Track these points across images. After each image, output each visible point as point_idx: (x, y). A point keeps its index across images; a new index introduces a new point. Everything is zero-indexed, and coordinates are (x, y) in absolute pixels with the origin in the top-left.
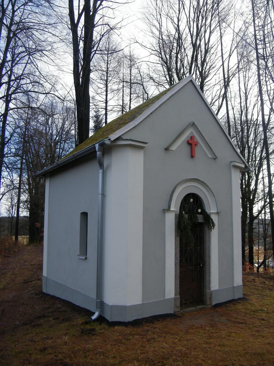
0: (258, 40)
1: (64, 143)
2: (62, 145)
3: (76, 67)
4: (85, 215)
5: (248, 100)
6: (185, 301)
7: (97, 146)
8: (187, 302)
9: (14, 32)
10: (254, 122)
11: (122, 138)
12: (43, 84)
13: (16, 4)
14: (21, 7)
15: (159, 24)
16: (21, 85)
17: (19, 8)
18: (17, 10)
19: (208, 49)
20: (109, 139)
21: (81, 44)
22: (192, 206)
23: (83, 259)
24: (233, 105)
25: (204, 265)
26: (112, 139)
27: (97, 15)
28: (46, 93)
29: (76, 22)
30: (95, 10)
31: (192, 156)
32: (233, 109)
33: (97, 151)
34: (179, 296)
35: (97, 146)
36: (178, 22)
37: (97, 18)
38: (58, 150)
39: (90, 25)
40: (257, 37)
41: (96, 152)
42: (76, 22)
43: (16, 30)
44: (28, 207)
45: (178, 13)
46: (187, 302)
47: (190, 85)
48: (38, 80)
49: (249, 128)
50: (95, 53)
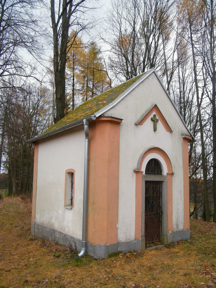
0: (193, 41)
1: (39, 116)
2: (37, 118)
3: (56, 57)
4: (71, 174)
5: (185, 86)
6: (148, 241)
7: (84, 121)
8: (150, 242)
9: (3, 27)
10: (189, 103)
11: (104, 115)
12: (24, 69)
13: (5, 5)
14: (9, 8)
15: (120, 25)
16: (7, 69)
17: (7, 8)
18: (6, 10)
19: (158, 45)
20: (95, 116)
21: (60, 40)
22: (154, 167)
23: (70, 209)
24: (174, 90)
25: (162, 213)
26: (97, 116)
27: (72, 17)
28: (27, 76)
29: (56, 22)
30: (71, 13)
31: (155, 130)
32: (174, 93)
33: (84, 124)
34: (144, 238)
35: (84, 121)
36: (134, 25)
37: (72, 18)
38: (33, 121)
39: (66, 25)
40: (193, 38)
41: (84, 126)
42: (56, 22)
43: (5, 26)
44: (7, 166)
45: (134, 17)
46: (150, 242)
47: (154, 74)
48: (21, 66)
49: (186, 108)
50: (71, 47)
